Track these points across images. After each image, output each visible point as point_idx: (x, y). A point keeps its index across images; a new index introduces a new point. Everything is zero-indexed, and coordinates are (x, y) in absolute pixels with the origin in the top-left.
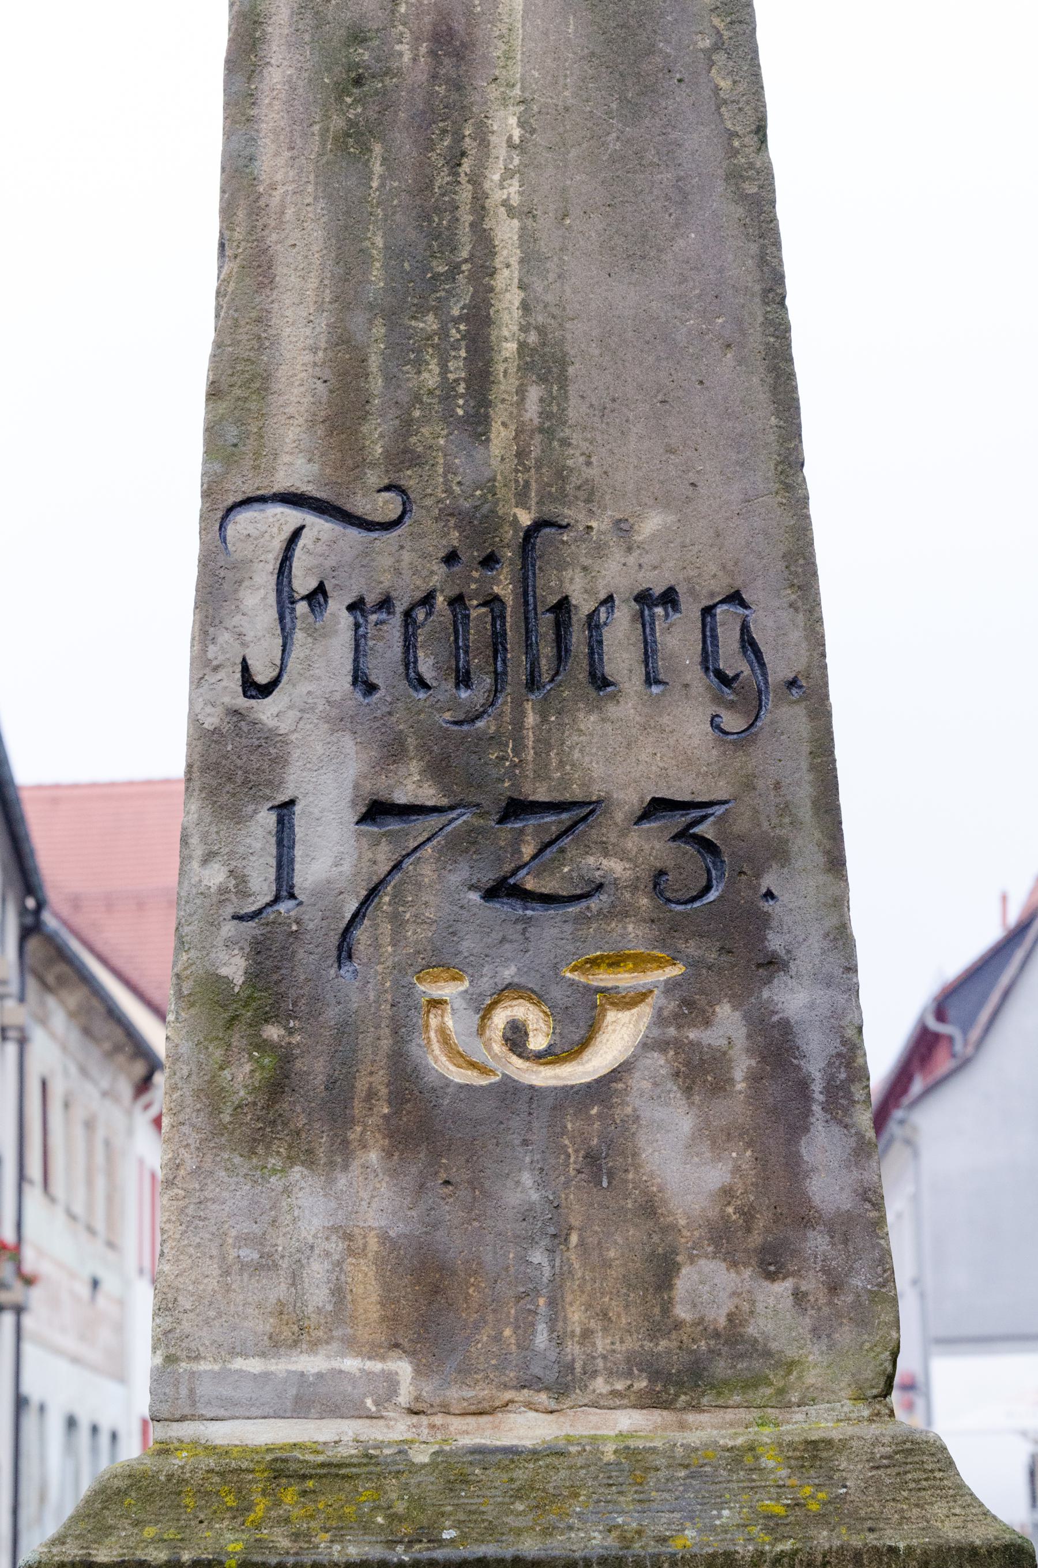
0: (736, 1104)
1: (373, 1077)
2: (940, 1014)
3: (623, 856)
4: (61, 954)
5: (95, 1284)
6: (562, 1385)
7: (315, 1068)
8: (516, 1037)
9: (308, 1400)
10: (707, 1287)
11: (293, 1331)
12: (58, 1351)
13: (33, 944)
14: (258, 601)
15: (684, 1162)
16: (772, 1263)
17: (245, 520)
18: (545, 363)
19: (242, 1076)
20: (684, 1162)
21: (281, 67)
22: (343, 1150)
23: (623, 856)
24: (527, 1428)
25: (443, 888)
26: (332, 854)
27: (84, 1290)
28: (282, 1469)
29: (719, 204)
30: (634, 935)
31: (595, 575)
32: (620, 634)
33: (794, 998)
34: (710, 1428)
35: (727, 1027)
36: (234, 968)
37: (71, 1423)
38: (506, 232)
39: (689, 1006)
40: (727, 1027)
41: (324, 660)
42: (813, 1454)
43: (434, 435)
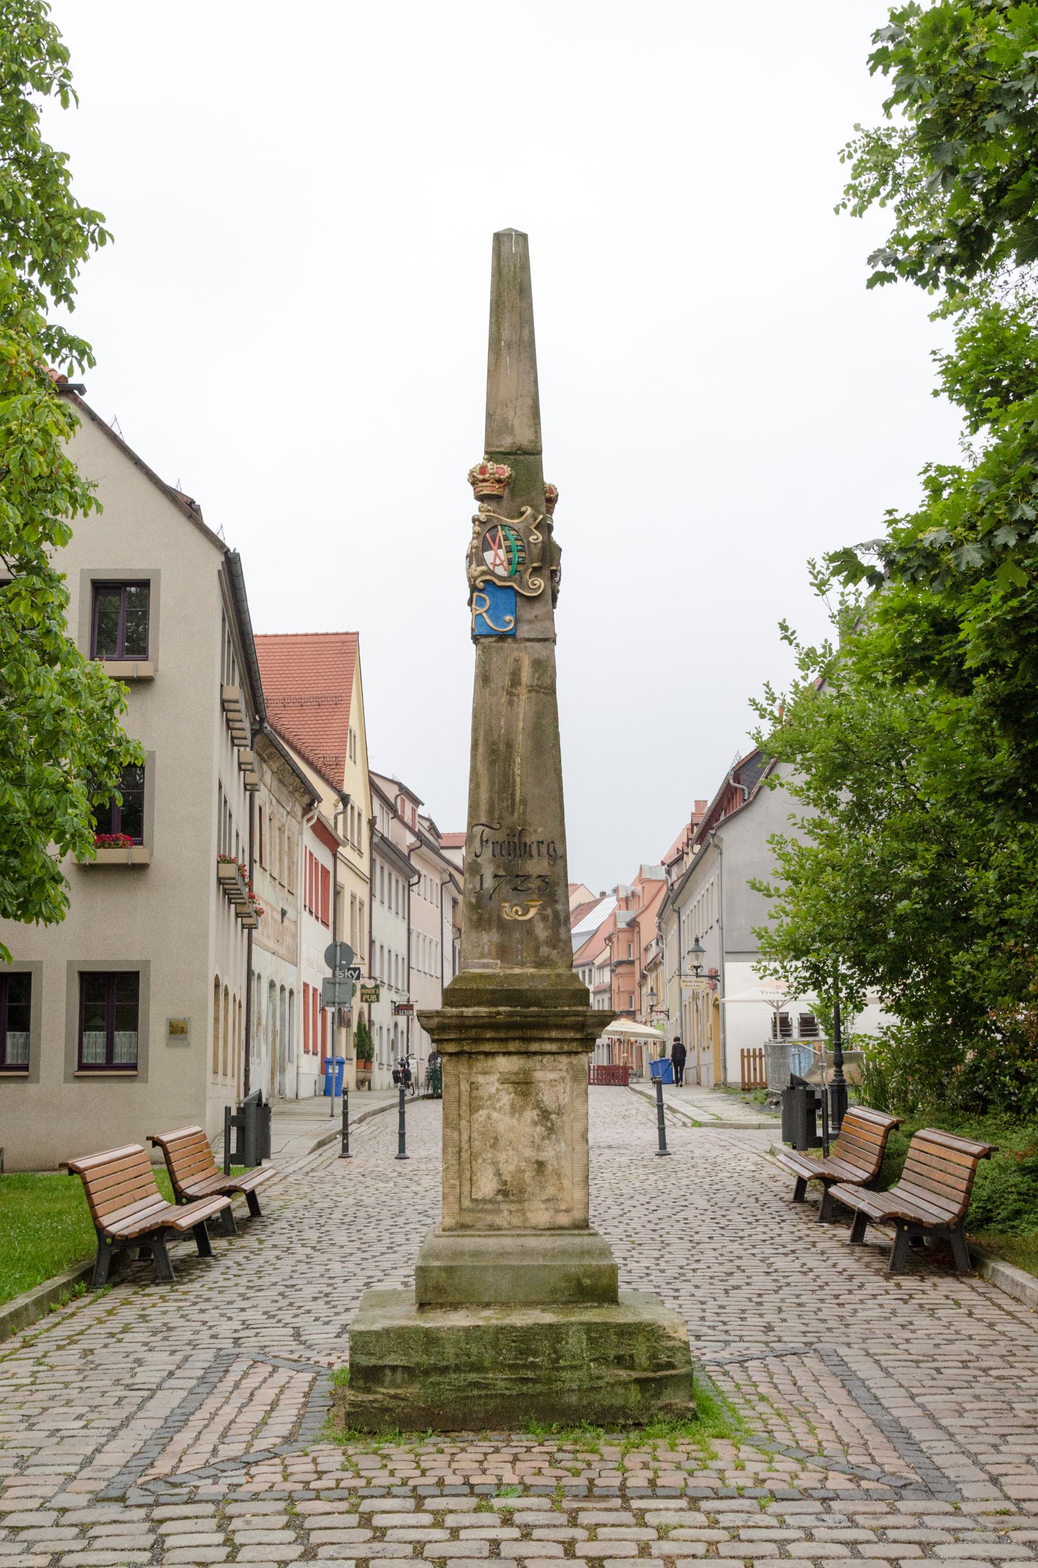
0: (549, 924)
1: (495, 917)
2: (737, 779)
3: (534, 884)
4: (272, 743)
5: (284, 913)
6: (523, 965)
7: (486, 916)
8: (516, 912)
9: (485, 966)
10: (544, 951)
11: (482, 956)
12: (266, 949)
13: (258, 738)
14: (477, 841)
15: (542, 932)
16: (554, 947)
17: (475, 829)
18: (524, 802)
19: (475, 917)
20: (542, 932)
21: (481, 749)
22: (490, 929)
23: (534, 884)
24: (517, 971)
25: (506, 889)
26: (489, 883)
27: (279, 917)
28: (481, 976)
29: (553, 775)
30: (535, 896)
31: (531, 839)
32: (534, 847)
33: (559, 907)
34: (544, 971)
35: (549, 911)
36: (474, 901)
37: (272, 985)
38: (518, 779)
39: (543, 908)
40: (549, 911)
41: (488, 852)
42: (559, 975)
43: (505, 814)
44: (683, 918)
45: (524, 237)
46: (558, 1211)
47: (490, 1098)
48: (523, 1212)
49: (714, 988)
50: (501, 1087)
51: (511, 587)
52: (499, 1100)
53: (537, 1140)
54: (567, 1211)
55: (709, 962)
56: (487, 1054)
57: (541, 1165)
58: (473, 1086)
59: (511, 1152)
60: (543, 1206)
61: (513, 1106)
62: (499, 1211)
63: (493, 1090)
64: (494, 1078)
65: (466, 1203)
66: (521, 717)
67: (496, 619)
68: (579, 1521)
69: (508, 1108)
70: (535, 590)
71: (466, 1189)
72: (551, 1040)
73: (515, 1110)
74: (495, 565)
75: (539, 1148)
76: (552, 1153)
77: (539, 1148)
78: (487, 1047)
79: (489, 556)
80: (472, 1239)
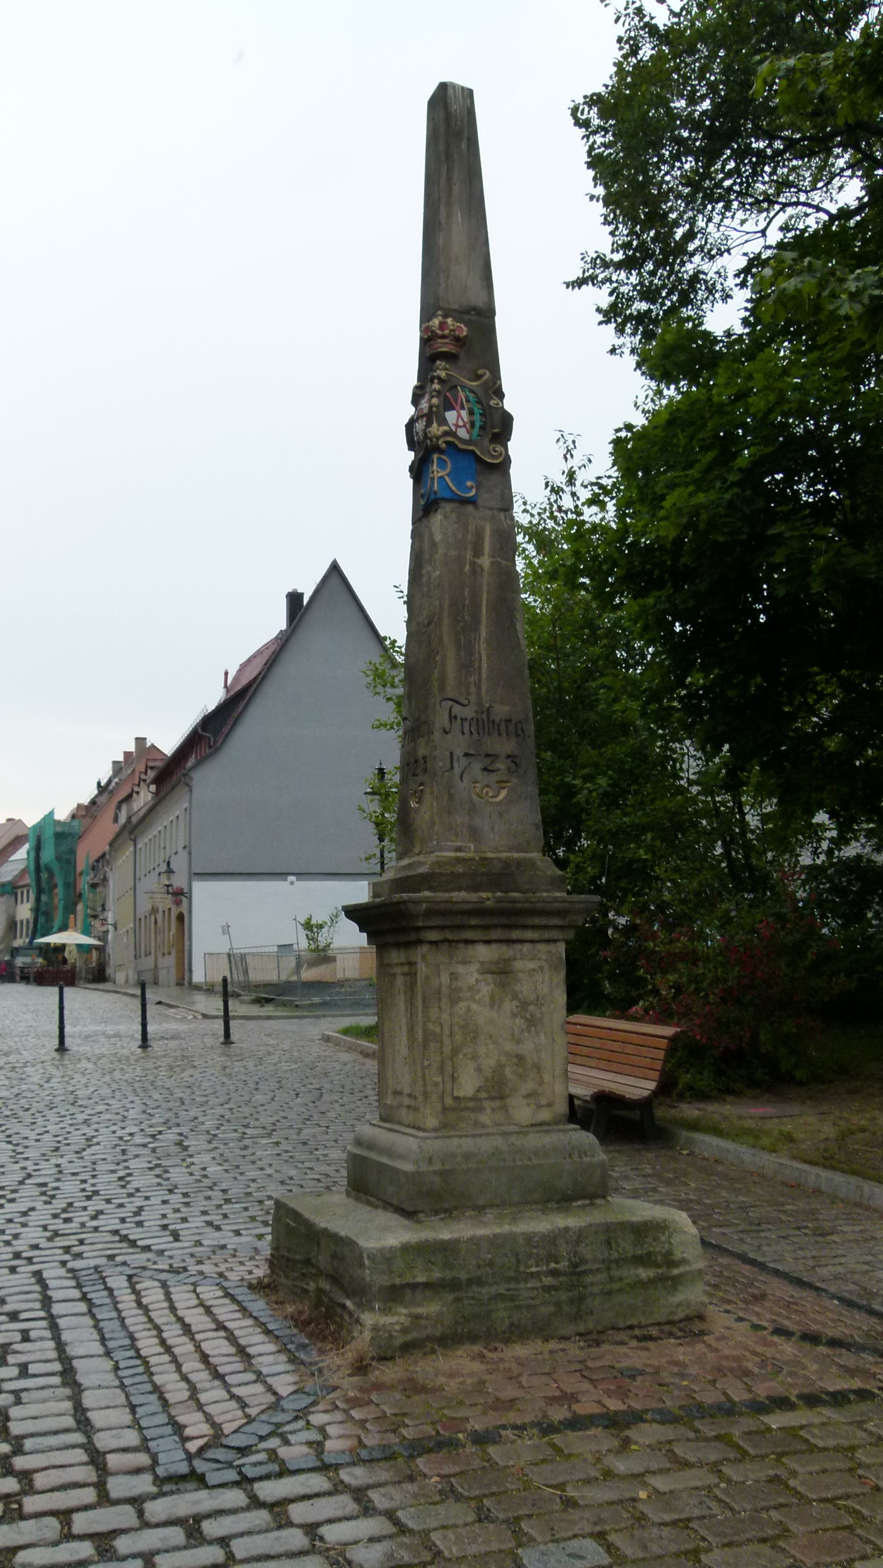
9: (459, 849)
44: (139, 846)
45: (470, 92)
46: (539, 1106)
47: (470, 988)
48: (505, 1108)
49: (178, 903)
50: (480, 977)
51: (473, 452)
52: (478, 991)
53: (517, 1032)
54: (549, 1105)
55: (179, 881)
56: (467, 942)
57: (520, 1058)
58: (454, 976)
59: (491, 1046)
60: (525, 1102)
61: (492, 998)
62: (481, 1109)
63: (472, 980)
64: (474, 968)
65: (449, 1101)
66: (485, 588)
67: (459, 484)
68: (30, 1372)
69: (487, 999)
70: (493, 457)
71: (449, 1086)
72: (534, 927)
73: (493, 1002)
74: (457, 426)
75: (518, 1042)
76: (532, 1046)
77: (518, 1042)
78: (469, 935)
79: (451, 416)
80: (404, 1138)
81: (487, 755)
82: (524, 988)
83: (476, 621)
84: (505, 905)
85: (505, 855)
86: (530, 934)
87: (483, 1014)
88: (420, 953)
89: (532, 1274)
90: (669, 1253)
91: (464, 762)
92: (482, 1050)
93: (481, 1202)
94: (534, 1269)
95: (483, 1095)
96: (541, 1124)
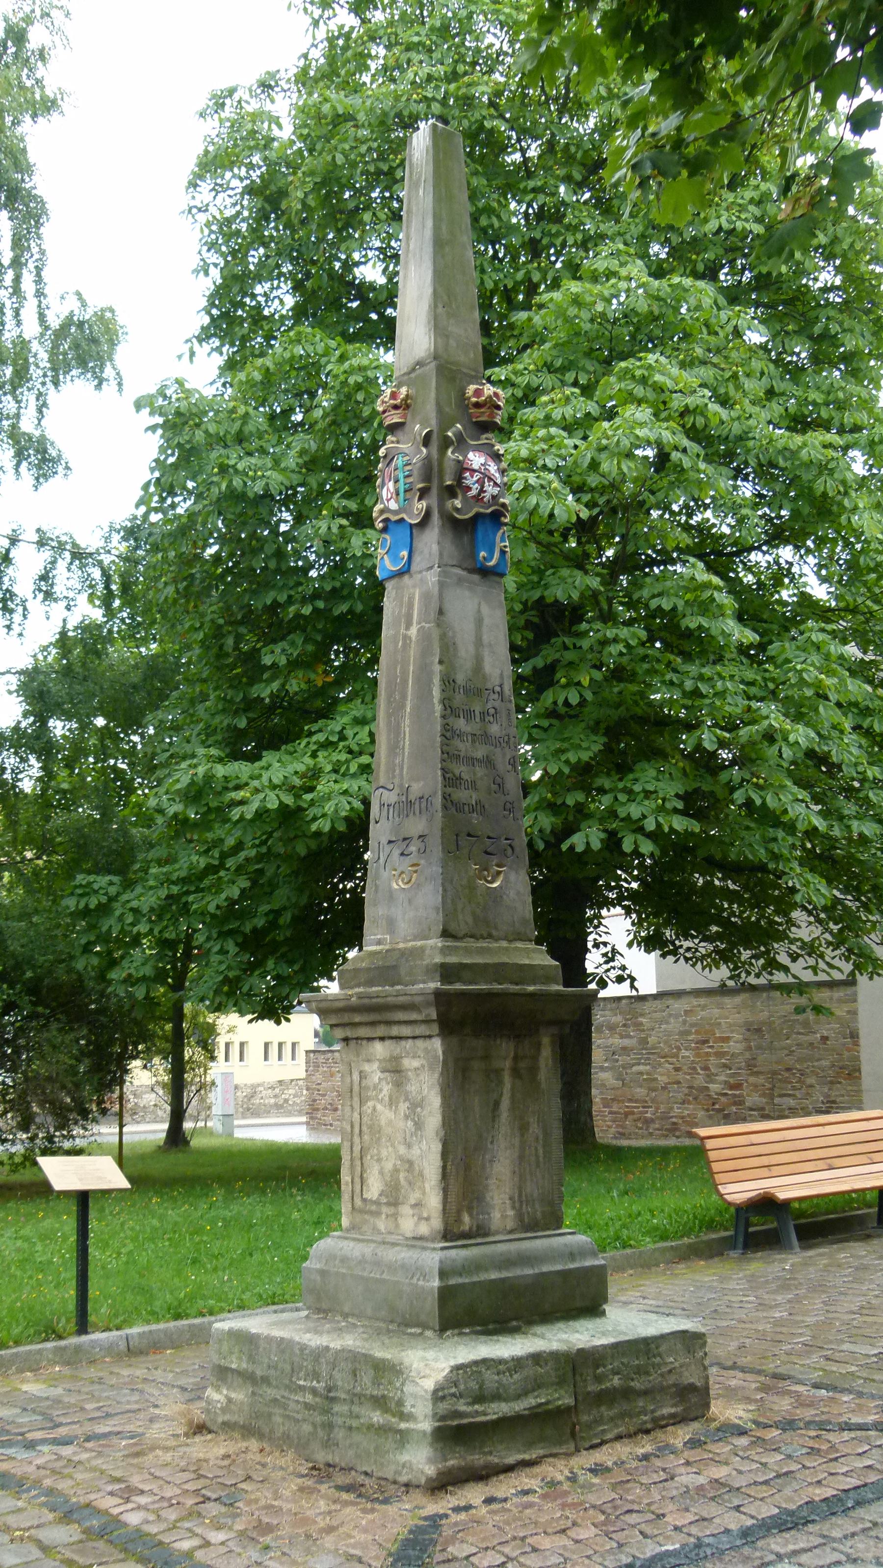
50: (382, 1076)
54: (427, 1219)
57: (411, 1163)
62: (378, 1214)
77: (409, 1146)
81: (405, 839)
82: (412, 1088)
83: (404, 697)
84: (366, 1001)
85: (410, 944)
86: (406, 1031)
87: (385, 1114)
88: (437, 1044)
89: (300, 1387)
90: (400, 1403)
91: (388, 849)
92: (384, 1153)
93: (346, 1309)
94: (302, 1383)
95: (384, 1200)
96: (421, 1238)
